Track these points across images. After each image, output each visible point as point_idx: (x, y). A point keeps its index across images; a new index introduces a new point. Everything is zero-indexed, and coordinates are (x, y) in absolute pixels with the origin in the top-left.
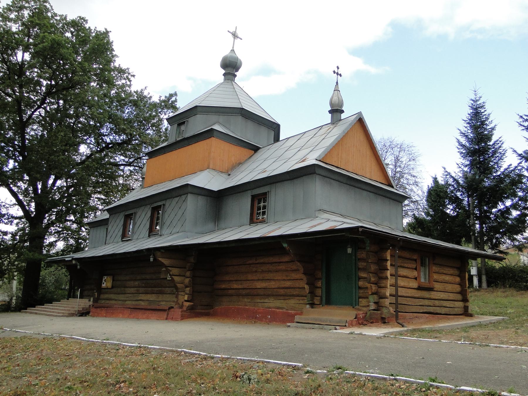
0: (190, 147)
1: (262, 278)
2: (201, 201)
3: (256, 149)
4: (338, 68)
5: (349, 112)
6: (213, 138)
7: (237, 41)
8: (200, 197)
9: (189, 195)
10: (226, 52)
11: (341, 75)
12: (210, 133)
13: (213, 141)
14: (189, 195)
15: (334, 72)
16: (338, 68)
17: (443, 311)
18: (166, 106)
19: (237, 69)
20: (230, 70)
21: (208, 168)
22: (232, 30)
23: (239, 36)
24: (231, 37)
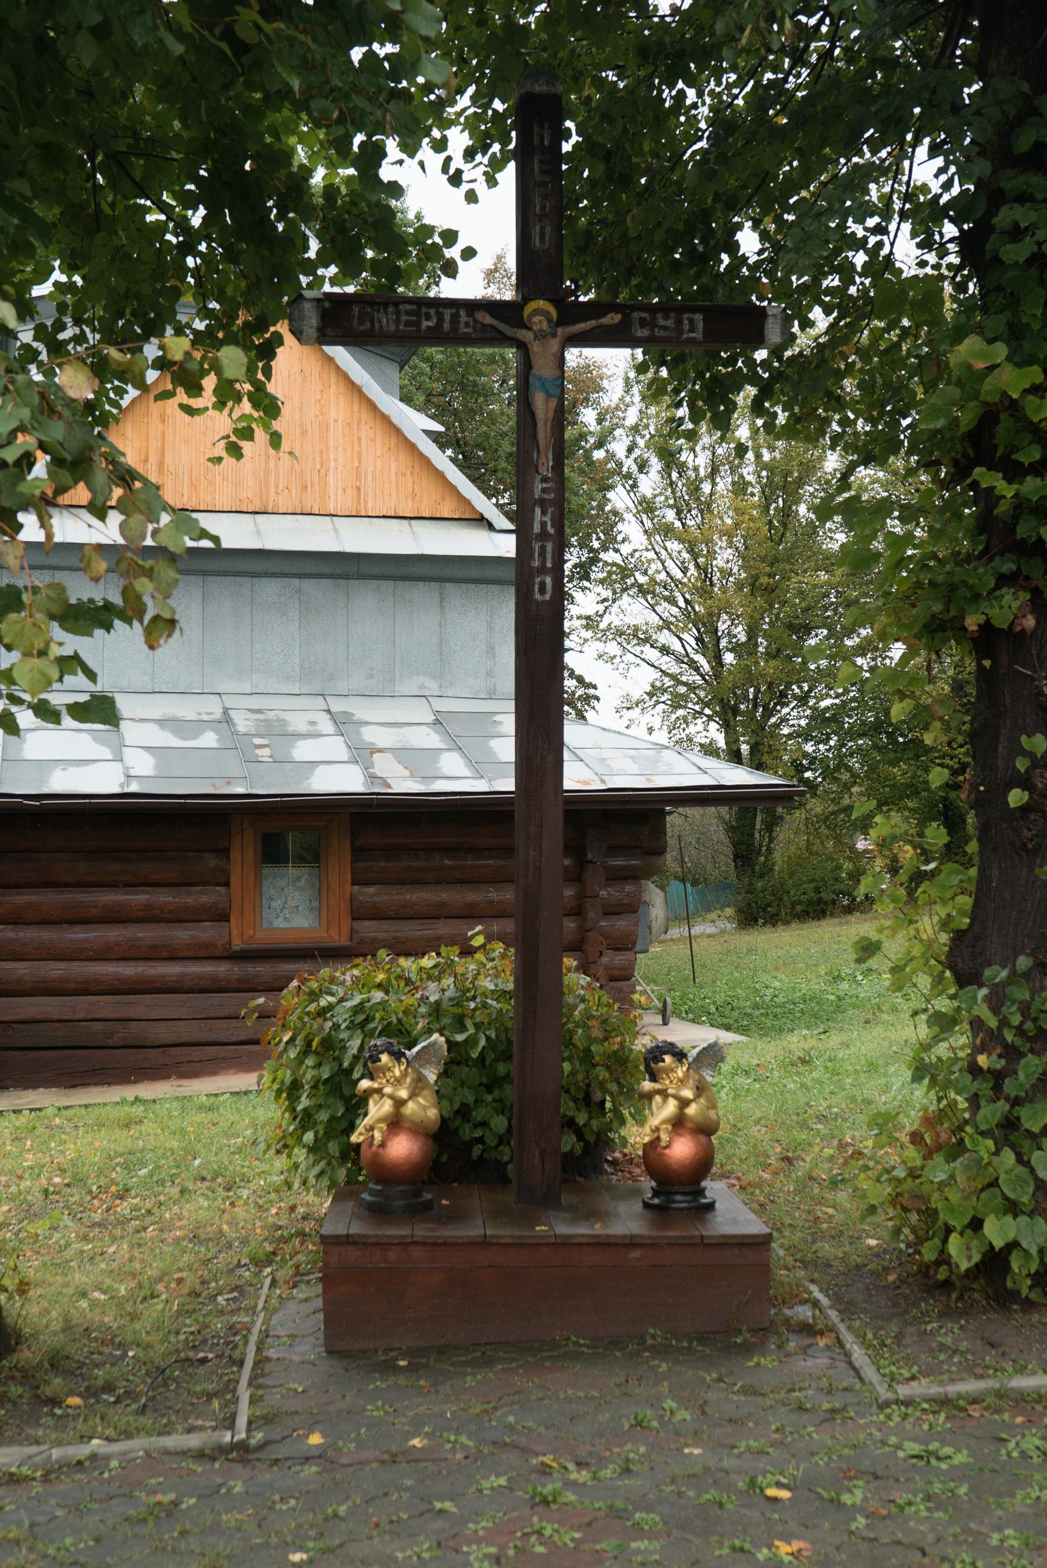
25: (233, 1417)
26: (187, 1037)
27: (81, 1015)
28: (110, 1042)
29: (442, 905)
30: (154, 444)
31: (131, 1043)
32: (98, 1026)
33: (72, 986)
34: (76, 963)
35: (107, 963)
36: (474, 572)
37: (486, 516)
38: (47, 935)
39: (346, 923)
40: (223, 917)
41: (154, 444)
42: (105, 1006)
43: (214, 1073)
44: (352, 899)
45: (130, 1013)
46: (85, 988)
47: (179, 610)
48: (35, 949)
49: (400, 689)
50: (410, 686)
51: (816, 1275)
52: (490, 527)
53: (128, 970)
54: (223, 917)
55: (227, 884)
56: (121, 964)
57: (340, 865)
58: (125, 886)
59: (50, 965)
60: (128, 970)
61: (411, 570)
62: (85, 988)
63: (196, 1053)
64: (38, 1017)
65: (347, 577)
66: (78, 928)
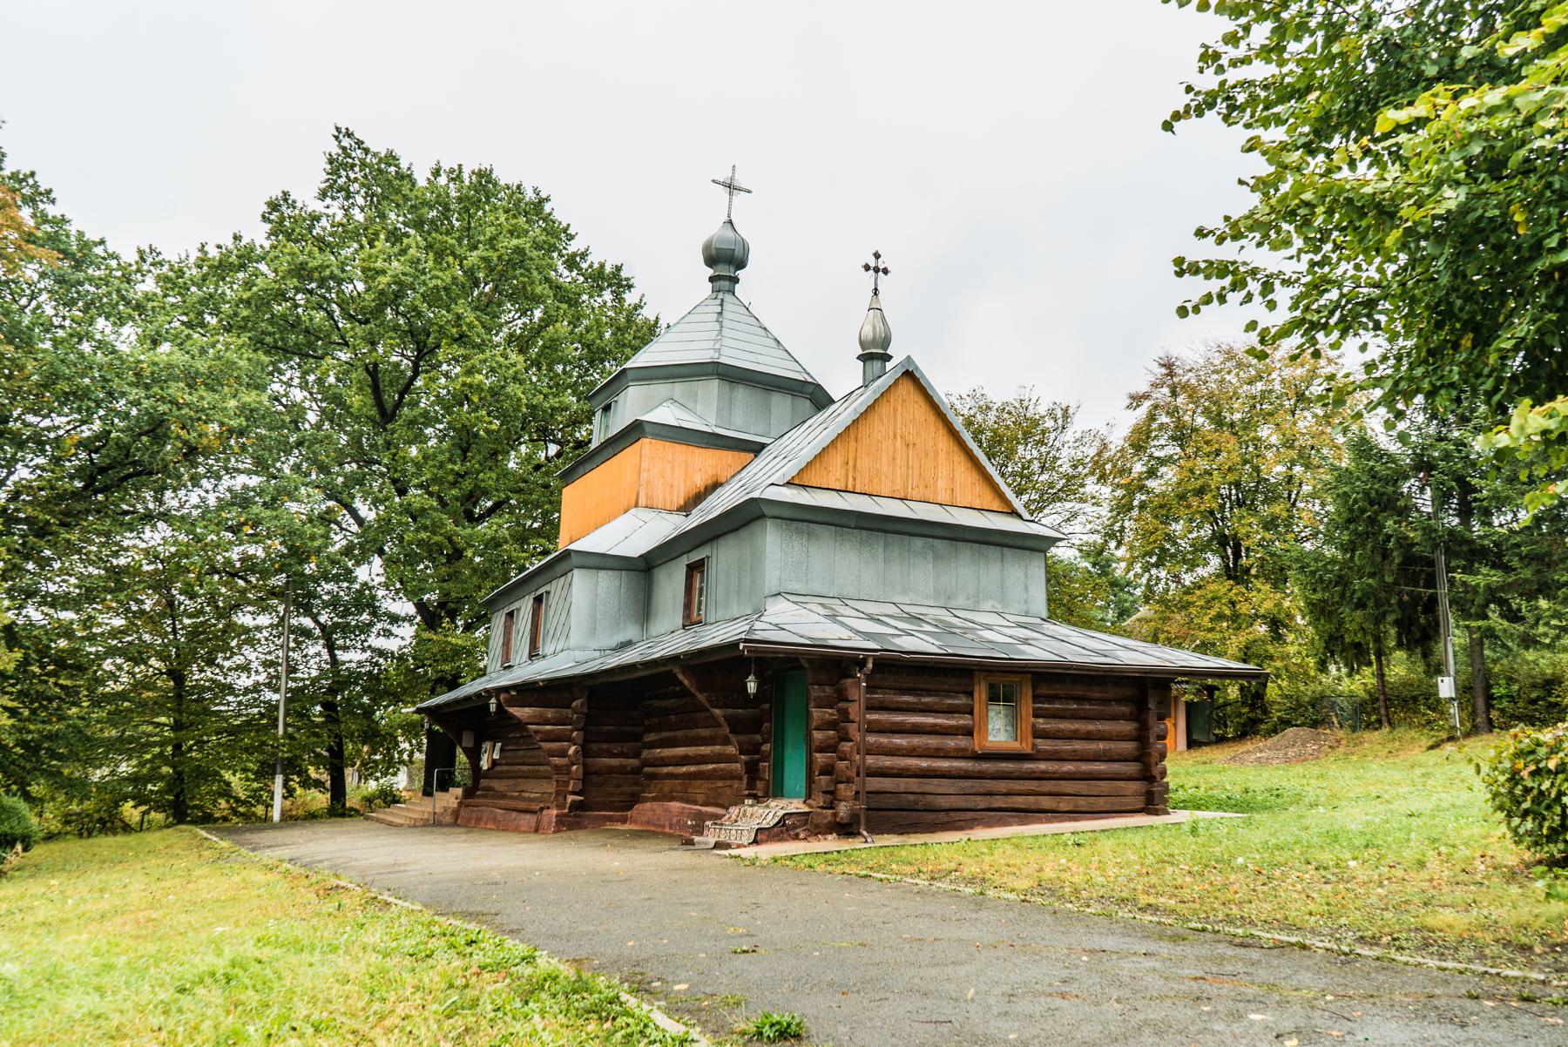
0: (697, 450)
1: (1105, 957)
2: (607, 582)
3: (763, 446)
4: (877, 256)
5: (898, 352)
6: (643, 440)
7: (739, 197)
8: (602, 574)
9: (576, 572)
10: (711, 229)
11: (886, 271)
12: (636, 430)
13: (646, 445)
14: (576, 572)
15: (867, 268)
16: (877, 256)
17: (1064, 805)
18: (193, 525)
19: (741, 265)
20: (724, 270)
21: (636, 505)
22: (724, 176)
23: (744, 186)
24: (723, 192)
26: (956, 805)
29: (1076, 731)
30: (851, 455)
32: (911, 797)
36: (940, 532)
38: (883, 740)
39: (1030, 740)
40: (969, 732)
41: (851, 455)
42: (913, 784)
43: (990, 826)
44: (1034, 725)
45: (927, 789)
49: (982, 607)
50: (987, 606)
51: (1049, 1025)
52: (1020, 517)
53: (924, 763)
54: (969, 732)
55: (971, 713)
57: (1027, 706)
60: (924, 763)
61: (991, 539)
63: (970, 815)
65: (956, 540)
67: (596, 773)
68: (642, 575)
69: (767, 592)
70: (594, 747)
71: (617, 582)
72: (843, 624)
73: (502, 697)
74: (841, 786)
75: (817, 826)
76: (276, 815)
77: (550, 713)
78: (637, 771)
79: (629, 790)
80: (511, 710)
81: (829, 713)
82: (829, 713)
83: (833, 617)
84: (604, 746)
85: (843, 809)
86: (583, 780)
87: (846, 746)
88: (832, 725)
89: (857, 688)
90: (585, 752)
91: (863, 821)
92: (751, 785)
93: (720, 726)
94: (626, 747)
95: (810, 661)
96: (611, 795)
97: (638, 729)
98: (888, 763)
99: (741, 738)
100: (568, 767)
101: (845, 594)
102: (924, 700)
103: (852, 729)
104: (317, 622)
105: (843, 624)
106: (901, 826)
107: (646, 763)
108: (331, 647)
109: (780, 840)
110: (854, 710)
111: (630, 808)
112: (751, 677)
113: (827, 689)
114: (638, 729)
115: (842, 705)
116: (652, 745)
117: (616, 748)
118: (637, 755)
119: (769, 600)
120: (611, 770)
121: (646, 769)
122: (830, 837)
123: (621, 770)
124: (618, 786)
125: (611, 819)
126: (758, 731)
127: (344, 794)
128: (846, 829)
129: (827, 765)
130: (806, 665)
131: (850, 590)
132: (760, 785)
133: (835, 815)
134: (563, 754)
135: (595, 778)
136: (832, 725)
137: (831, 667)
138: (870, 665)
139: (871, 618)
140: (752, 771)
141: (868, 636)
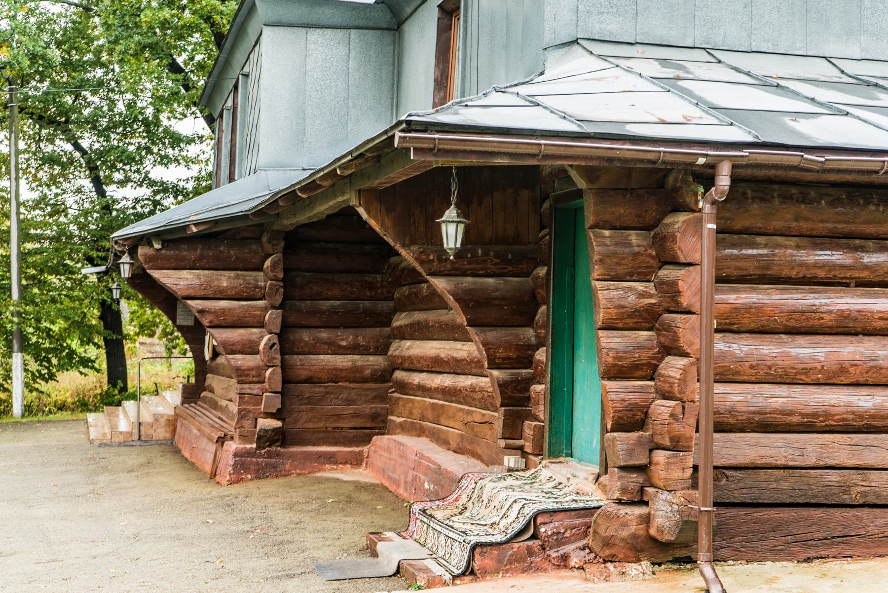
8: (315, 35)
25: (271, 458)
27: (811, 461)
28: (847, 499)
31: (871, 500)
32: (833, 477)
33: (796, 419)
34: (799, 389)
35: (835, 389)
36: (447, 129)
37: (152, 217)
38: (769, 349)
42: (839, 448)
46: (811, 425)
47: (549, 60)
48: (752, 367)
56: (852, 390)
58: (858, 285)
59: (768, 389)
62: (811, 425)
64: (759, 462)
66: (801, 340)
67: (309, 380)
68: (388, 37)
69: (548, 38)
70: (306, 336)
71: (342, 50)
72: (687, 94)
73: (141, 251)
74: (660, 456)
75: (607, 543)
76: (17, 408)
77: (225, 279)
78: (384, 376)
79: (367, 408)
80: (156, 274)
81: (633, 294)
82: (633, 294)
83: (670, 84)
84: (324, 334)
85: (665, 511)
86: (283, 393)
87: (673, 367)
88: (646, 318)
89: (696, 235)
90: (286, 343)
91: (704, 540)
92: (512, 428)
93: (445, 306)
94: (364, 336)
95: (590, 173)
96: (339, 417)
97: (384, 306)
98: (778, 403)
99: (492, 335)
100: (259, 371)
101: (718, 40)
102: (869, 259)
103: (688, 330)
104: (77, 147)
105: (687, 94)
106: (805, 543)
107: (394, 366)
108: (98, 183)
109: (528, 569)
110: (692, 284)
111: (367, 440)
112: (451, 213)
113: (634, 237)
114: (384, 306)
115: (667, 273)
116: (403, 334)
117: (346, 338)
118: (382, 350)
119: (553, 56)
120: (335, 376)
121: (399, 375)
122: (633, 569)
123: (354, 376)
124: (350, 402)
125: (331, 459)
126: (529, 321)
127: (124, 376)
128: (672, 552)
129: (632, 408)
130: (581, 183)
131: (734, 36)
132: (529, 427)
133: (647, 520)
134: (250, 349)
135: (307, 389)
136: (646, 318)
137: (650, 184)
138: (724, 181)
139: (765, 83)
140: (515, 400)
141: (731, 115)
